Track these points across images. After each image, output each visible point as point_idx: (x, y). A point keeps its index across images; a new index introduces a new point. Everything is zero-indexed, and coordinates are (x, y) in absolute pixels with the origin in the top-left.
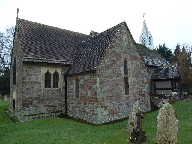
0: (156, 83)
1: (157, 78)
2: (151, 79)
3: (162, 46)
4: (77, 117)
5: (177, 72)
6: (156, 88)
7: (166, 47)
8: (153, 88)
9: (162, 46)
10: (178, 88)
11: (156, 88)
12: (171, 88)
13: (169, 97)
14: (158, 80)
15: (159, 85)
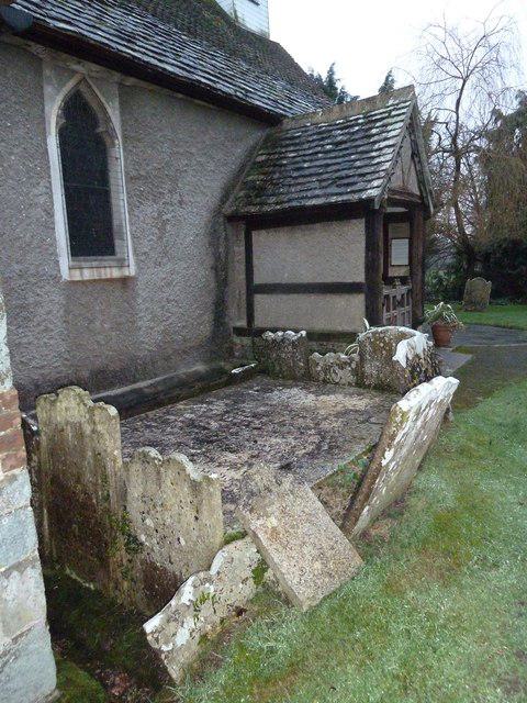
0: (260, 238)
1: (262, 204)
2: (217, 212)
3: (324, 77)
4: (370, 490)
5: (407, 152)
6: (258, 279)
7: (338, 85)
8: (239, 276)
9: (324, 77)
10: (404, 280)
11: (258, 279)
12: (360, 278)
13: (342, 366)
14: (266, 215)
15: (280, 255)
